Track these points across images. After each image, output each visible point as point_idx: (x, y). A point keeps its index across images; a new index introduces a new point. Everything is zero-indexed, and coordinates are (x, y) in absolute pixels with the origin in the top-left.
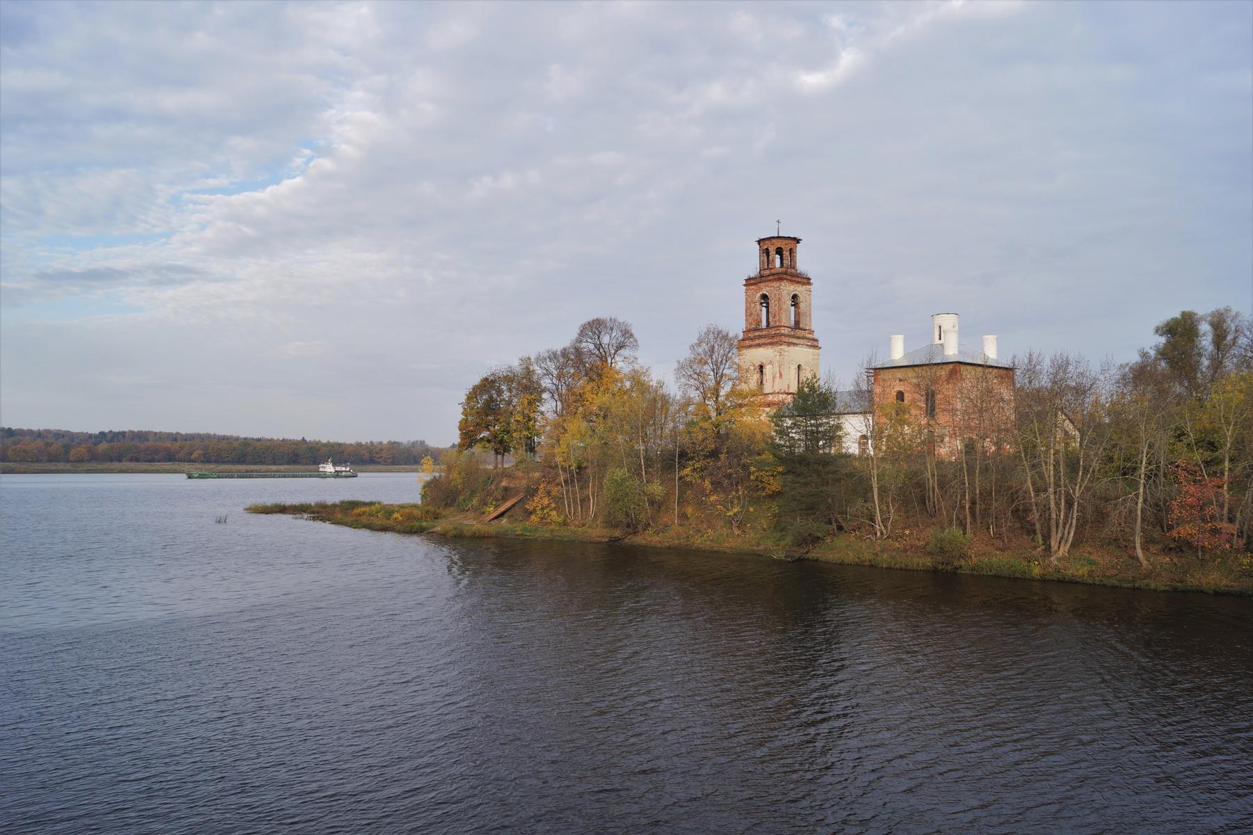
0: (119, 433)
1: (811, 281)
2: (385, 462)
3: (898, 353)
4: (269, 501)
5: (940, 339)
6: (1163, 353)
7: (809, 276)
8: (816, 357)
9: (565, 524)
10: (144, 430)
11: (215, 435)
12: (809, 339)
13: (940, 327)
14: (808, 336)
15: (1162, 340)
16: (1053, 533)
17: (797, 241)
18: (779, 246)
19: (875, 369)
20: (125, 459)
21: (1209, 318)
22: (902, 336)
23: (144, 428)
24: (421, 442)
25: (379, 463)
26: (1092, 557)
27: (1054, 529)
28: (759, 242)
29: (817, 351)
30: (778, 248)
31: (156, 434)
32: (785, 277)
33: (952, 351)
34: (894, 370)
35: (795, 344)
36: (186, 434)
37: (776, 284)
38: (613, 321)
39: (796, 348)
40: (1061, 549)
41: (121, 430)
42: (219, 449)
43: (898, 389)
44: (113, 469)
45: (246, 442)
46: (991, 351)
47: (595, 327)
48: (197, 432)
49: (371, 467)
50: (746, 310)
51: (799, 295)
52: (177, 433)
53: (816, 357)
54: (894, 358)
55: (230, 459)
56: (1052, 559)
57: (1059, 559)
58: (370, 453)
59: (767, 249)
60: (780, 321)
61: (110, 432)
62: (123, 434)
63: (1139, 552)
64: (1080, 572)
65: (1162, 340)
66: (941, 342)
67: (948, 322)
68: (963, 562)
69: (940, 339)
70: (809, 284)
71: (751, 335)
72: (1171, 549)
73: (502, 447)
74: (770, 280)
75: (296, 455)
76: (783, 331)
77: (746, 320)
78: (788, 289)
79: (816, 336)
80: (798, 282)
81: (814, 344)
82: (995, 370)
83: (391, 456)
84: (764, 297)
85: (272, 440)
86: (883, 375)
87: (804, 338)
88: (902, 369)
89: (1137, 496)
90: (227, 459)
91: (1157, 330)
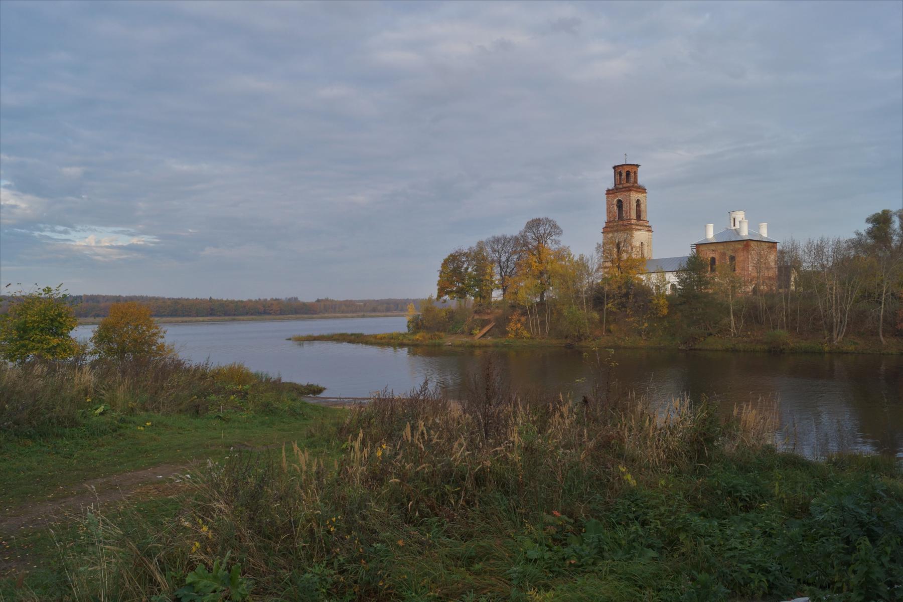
0: (77, 297)
1: (647, 191)
2: (274, 313)
3: (710, 234)
4: (304, 334)
5: (734, 226)
6: (869, 233)
7: (646, 188)
8: (650, 237)
9: (532, 338)
10: (94, 294)
11: (147, 296)
12: (646, 226)
13: (734, 219)
14: (646, 224)
15: (870, 226)
16: (834, 330)
17: (638, 166)
18: (628, 170)
19: (696, 245)
20: (91, 315)
21: (898, 214)
22: (712, 225)
23: (132, 294)
24: (295, 298)
25: (270, 314)
26: (855, 341)
27: (835, 327)
28: (614, 168)
29: (651, 233)
30: (627, 171)
31: (104, 297)
32: (632, 189)
33: (745, 233)
34: (709, 245)
35: (639, 230)
36: (127, 297)
37: (627, 194)
38: (547, 219)
39: (640, 232)
40: (839, 338)
41: (78, 295)
42: (158, 306)
43: (712, 256)
44: (88, 323)
45: (176, 301)
46: (764, 233)
47: (535, 224)
48: (134, 295)
49: (268, 317)
50: (607, 209)
51: (640, 199)
52: (120, 296)
53: (650, 237)
54: (708, 238)
55: (166, 313)
56: (834, 342)
57: (837, 342)
58: (264, 307)
59: (620, 172)
60: (630, 216)
61: (85, 295)
62: (80, 297)
63: (882, 339)
64: (851, 348)
65: (870, 226)
66: (735, 228)
67: (740, 216)
68: (785, 347)
69: (734, 226)
70: (645, 192)
71: (611, 224)
72: (896, 335)
73: (462, 293)
74: (624, 191)
75: (212, 310)
76: (632, 222)
77: (607, 215)
78: (634, 196)
79: (650, 224)
80: (640, 192)
81: (649, 229)
82: (767, 244)
83: (279, 309)
84: (619, 201)
85: (187, 300)
86: (701, 248)
87: (644, 226)
88: (713, 244)
89: (881, 308)
90: (163, 314)
91: (868, 220)
